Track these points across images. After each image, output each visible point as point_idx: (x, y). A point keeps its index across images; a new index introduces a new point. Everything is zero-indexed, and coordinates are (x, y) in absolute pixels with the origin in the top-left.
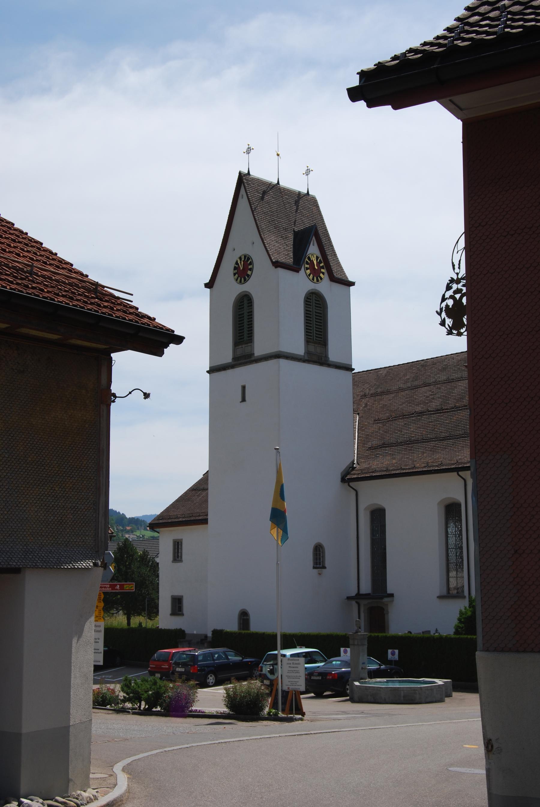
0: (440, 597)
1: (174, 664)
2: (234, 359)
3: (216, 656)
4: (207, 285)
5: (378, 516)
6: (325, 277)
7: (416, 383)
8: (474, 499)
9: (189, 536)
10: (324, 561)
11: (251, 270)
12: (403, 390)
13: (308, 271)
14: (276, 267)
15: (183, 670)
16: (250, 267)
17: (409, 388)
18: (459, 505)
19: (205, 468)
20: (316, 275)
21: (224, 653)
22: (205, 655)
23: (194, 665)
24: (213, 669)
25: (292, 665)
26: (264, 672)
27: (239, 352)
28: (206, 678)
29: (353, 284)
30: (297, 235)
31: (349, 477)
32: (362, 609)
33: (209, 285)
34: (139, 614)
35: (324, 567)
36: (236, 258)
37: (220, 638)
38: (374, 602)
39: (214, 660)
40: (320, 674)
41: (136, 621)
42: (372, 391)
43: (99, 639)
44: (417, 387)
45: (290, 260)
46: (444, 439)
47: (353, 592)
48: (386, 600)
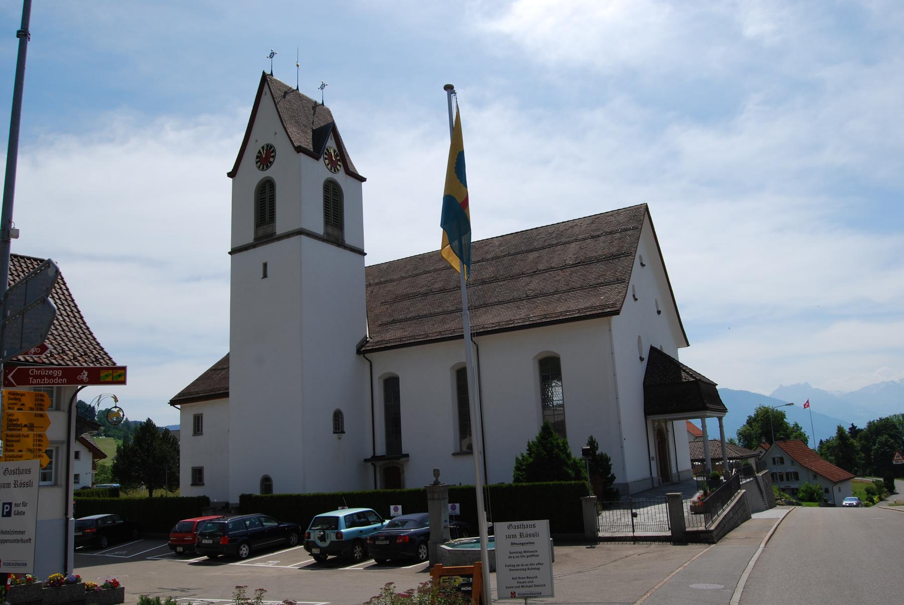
0: (454, 454)
1: (200, 535)
2: (255, 239)
3: (248, 523)
4: (231, 175)
5: (392, 385)
6: (342, 169)
7: (415, 272)
8: (107, 553)
9: (210, 410)
10: (342, 427)
11: (274, 157)
12: (405, 278)
13: (327, 161)
15: (211, 542)
16: (271, 160)
17: (410, 276)
22: (234, 523)
23: (224, 536)
25: (518, 540)
26: (312, 539)
27: (261, 232)
28: (239, 549)
29: (363, 180)
30: (314, 132)
31: (363, 350)
32: (378, 470)
33: (231, 175)
34: (161, 487)
36: (259, 148)
37: (247, 503)
38: (390, 462)
39: (247, 528)
40: (387, 537)
41: (158, 493)
42: (376, 281)
43: (25, 504)
44: (417, 275)
45: (310, 147)
46: (452, 312)
47: (369, 455)
48: (403, 459)
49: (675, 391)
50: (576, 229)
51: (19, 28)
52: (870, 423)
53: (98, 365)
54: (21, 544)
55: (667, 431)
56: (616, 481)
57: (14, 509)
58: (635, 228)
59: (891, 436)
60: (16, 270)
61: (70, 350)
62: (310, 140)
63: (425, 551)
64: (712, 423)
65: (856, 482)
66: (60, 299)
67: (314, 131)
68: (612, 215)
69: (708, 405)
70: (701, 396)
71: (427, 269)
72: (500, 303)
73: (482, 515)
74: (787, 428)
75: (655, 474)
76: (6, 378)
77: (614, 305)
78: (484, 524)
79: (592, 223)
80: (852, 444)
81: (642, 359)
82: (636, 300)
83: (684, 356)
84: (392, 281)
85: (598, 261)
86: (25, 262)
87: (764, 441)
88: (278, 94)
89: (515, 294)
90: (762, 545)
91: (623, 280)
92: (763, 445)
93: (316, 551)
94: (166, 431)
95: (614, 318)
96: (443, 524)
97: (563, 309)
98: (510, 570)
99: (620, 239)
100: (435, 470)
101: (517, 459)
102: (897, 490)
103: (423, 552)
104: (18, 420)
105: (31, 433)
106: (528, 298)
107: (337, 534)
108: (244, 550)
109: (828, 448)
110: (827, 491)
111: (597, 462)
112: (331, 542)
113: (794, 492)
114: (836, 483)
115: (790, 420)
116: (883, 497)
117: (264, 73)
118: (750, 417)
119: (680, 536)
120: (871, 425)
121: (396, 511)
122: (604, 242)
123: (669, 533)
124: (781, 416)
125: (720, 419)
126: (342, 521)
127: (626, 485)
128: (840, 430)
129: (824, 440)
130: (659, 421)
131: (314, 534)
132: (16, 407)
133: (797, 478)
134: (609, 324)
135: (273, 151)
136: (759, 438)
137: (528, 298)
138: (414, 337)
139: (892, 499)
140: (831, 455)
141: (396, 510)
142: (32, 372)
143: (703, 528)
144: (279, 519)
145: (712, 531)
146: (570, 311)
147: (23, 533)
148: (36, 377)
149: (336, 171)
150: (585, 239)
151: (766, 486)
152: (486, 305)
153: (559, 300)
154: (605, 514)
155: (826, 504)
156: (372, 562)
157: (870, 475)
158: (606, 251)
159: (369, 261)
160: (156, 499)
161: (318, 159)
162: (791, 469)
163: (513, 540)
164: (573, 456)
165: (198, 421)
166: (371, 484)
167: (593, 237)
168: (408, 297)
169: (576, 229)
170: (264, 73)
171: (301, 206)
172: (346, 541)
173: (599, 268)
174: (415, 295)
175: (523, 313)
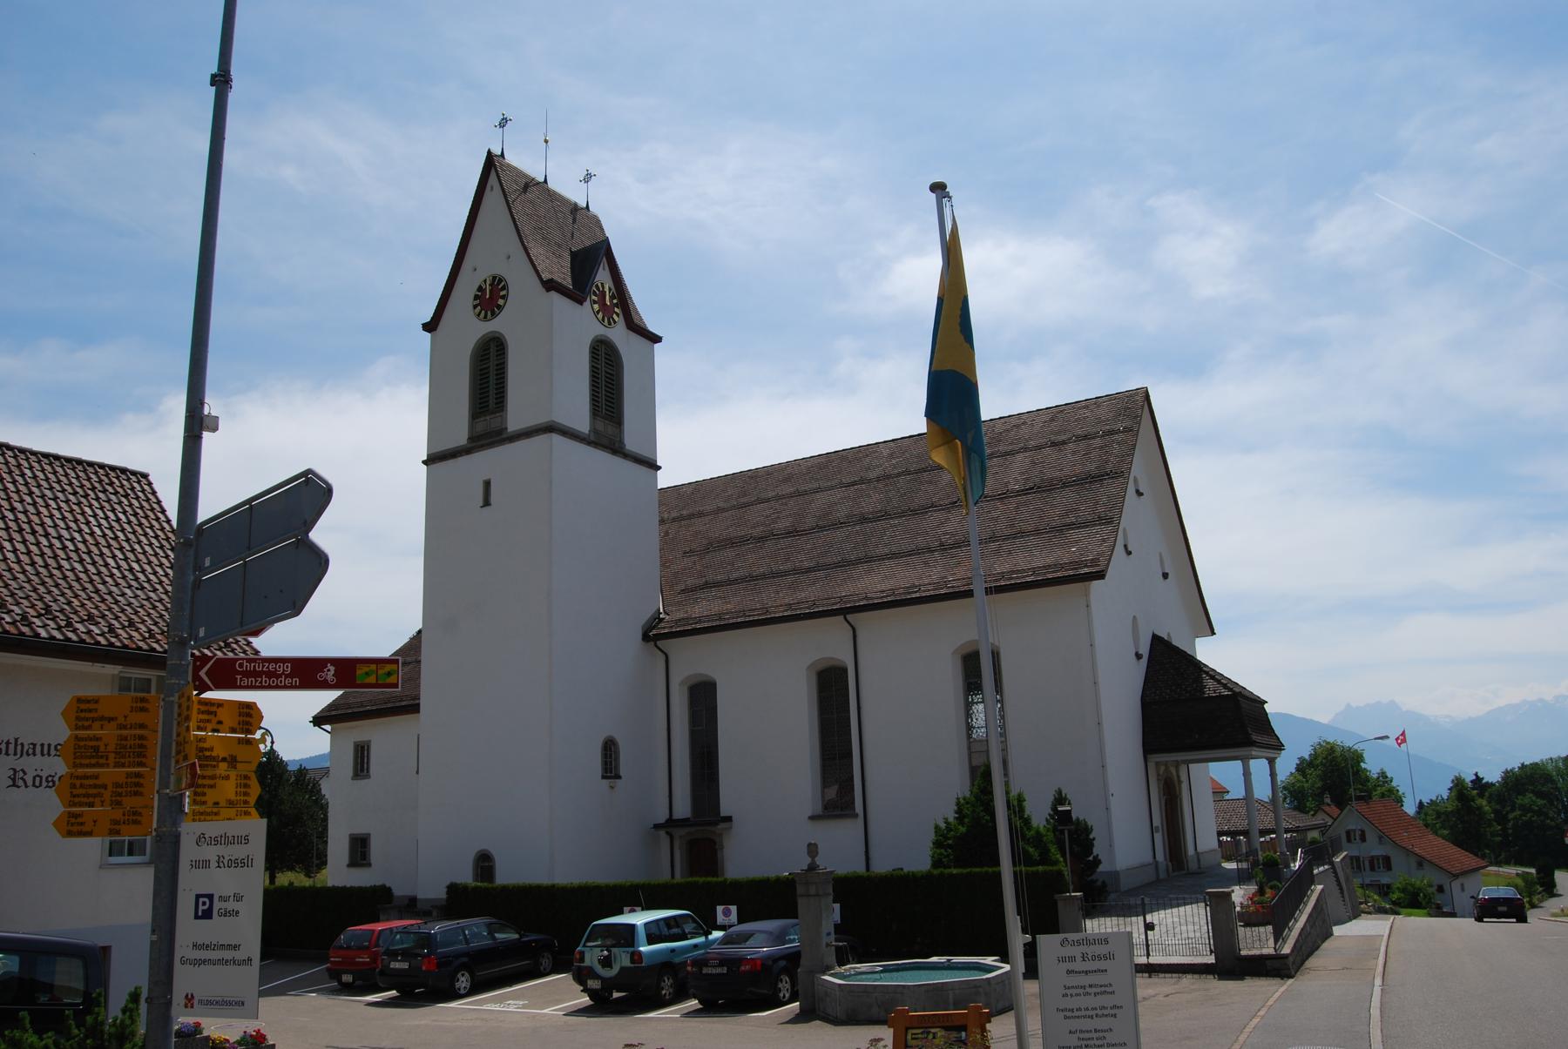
0: (812, 818)
2: (471, 439)
5: (703, 696)
6: (619, 320)
7: (742, 500)
9: (385, 736)
10: (617, 767)
12: (723, 510)
13: (596, 307)
14: (548, 290)
15: (405, 966)
16: (501, 302)
18: (844, 670)
19: (416, 623)
20: (606, 314)
21: (489, 925)
24: (465, 959)
25: (1079, 965)
26: (587, 963)
27: (481, 427)
28: (454, 979)
29: (656, 339)
31: (653, 634)
32: (677, 844)
33: (429, 327)
34: (291, 869)
35: (619, 777)
37: (459, 901)
38: (699, 830)
40: (722, 963)
42: (674, 514)
43: (238, 898)
45: (568, 282)
46: (809, 570)
47: (662, 817)
48: (722, 826)
49: (1194, 711)
50: (1024, 430)
51: (215, 70)
52: (1506, 772)
53: (231, 655)
54: (231, 968)
55: (1180, 782)
56: (1101, 868)
57: (217, 905)
58: (1127, 430)
59: (1540, 795)
60: (82, 486)
61: (143, 622)
62: (567, 270)
63: (788, 986)
64: (1259, 766)
65: (1488, 875)
66: (157, 537)
67: (574, 255)
68: (1086, 407)
69: (1254, 737)
70: (1237, 721)
71: (763, 496)
72: (894, 556)
73: (1013, 923)
74: (1367, 779)
75: (1160, 857)
76: (196, 677)
77: (1094, 562)
78: (1017, 939)
79: (1052, 420)
80: (1480, 808)
81: (1139, 656)
82: (1129, 553)
83: (1207, 652)
84: (701, 514)
85: (1065, 485)
86: (96, 473)
87: (1328, 800)
88: (511, 187)
89: (921, 541)
90: (1378, 981)
91: (1108, 519)
92: (1327, 808)
93: (594, 984)
94: (302, 772)
95: (1096, 584)
96: (825, 940)
97: (1006, 567)
98: (1066, 1017)
99: (1101, 448)
100: (810, 845)
101: (937, 827)
102: (1559, 889)
103: (785, 987)
104: (211, 749)
105: (233, 774)
106: (943, 547)
107: (633, 954)
108: (463, 982)
109: (1439, 815)
110: (1441, 889)
111: (1072, 835)
112: (622, 969)
113: (1384, 891)
114: (1456, 876)
115: (1372, 766)
116: (1535, 900)
117: (489, 152)
118: (1302, 760)
119: (1230, 965)
120: (1508, 774)
121: (727, 914)
122: (1074, 453)
123: (1211, 960)
124: (1357, 757)
125: (1271, 762)
126: (641, 934)
127: (1115, 875)
128: (1458, 784)
129: (1425, 800)
130: (1166, 764)
131: (592, 955)
132: (210, 726)
133: (1389, 868)
134: (1087, 594)
135: (503, 288)
136: (1318, 796)
137: (943, 547)
138: (743, 613)
139: (1552, 904)
140: (1443, 827)
141: (727, 913)
142: (241, 665)
143: (1271, 951)
144: (524, 928)
145: (1286, 957)
146: (1018, 571)
147: (236, 947)
148: (247, 674)
149: (612, 322)
150: (1039, 448)
151: (1347, 880)
152: (868, 559)
153: (997, 552)
154: (1088, 923)
155: (1439, 912)
156: (693, 1003)
157: (1507, 863)
158: (1078, 469)
159: (665, 480)
160: (282, 890)
161: (581, 302)
162: (1378, 851)
163: (1071, 966)
164: (1035, 823)
165: (362, 754)
166: (665, 867)
167: (1054, 444)
168: (731, 543)
169: (1024, 430)
170: (489, 152)
171: (551, 383)
172: (650, 968)
173: (1067, 497)
174: (744, 540)
175: (934, 574)
